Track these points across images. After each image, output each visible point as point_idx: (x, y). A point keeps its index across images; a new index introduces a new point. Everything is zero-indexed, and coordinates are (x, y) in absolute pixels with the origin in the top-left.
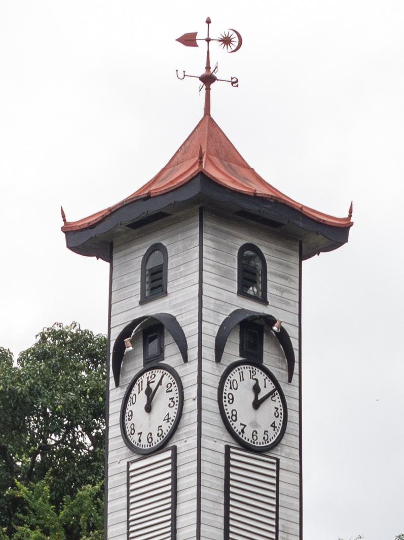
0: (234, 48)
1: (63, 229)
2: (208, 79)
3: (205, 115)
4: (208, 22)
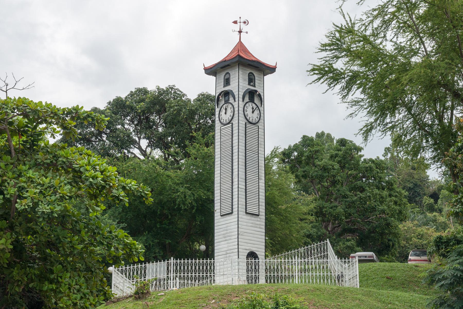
2: (240, 32)
4: (240, 18)
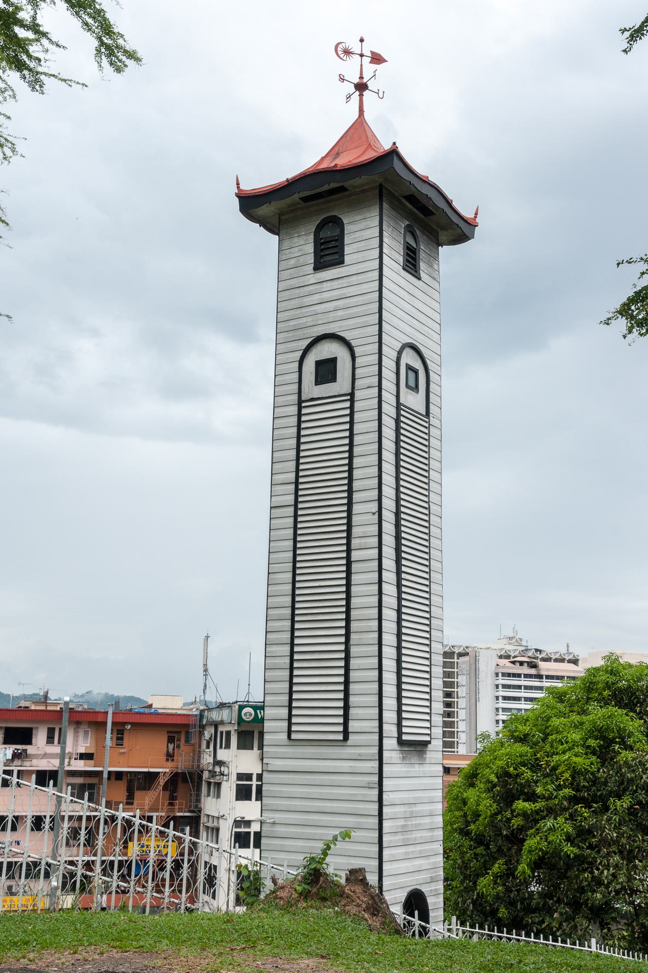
0: (340, 46)
1: (237, 195)
2: (361, 87)
3: (359, 116)
4: (362, 40)
